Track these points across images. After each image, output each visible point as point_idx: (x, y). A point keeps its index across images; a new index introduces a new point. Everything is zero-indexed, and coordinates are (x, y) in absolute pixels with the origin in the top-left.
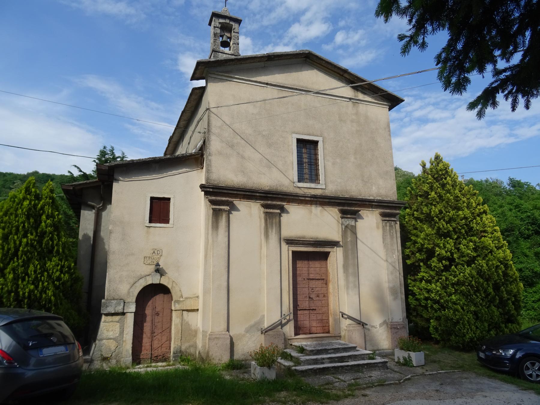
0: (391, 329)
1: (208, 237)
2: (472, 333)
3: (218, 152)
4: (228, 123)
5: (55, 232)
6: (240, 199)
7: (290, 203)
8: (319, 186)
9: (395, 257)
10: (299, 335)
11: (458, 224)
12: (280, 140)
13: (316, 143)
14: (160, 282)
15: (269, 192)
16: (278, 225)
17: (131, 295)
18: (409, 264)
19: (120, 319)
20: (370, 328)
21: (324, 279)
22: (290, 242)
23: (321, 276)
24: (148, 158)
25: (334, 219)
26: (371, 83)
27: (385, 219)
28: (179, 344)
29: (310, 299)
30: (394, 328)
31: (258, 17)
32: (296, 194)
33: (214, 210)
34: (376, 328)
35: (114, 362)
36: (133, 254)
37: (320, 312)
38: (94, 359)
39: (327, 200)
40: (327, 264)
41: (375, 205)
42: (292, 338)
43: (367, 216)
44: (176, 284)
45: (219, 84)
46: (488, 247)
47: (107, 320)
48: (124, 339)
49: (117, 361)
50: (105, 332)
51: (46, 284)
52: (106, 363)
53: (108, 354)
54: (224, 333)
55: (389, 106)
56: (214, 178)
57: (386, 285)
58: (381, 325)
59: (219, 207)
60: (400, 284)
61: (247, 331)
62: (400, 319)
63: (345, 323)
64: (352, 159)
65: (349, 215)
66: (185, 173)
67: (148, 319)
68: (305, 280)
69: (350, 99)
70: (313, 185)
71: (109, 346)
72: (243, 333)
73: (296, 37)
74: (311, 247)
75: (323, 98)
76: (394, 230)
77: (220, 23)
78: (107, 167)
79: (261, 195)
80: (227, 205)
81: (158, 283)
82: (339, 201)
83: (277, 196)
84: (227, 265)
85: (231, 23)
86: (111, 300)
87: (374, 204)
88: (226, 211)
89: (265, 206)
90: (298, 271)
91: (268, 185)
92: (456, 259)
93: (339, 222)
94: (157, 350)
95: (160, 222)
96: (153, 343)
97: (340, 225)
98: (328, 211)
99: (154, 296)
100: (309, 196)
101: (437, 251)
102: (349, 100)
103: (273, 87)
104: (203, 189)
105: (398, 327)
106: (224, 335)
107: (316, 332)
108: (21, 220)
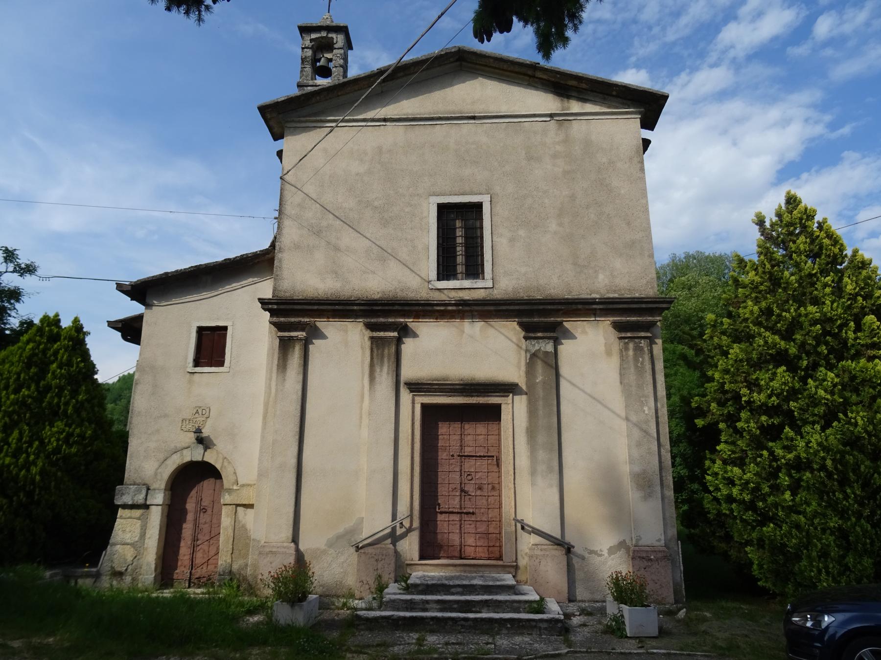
0: (633, 558)
1: (270, 385)
2: (830, 579)
3: (294, 244)
4: (314, 196)
5: (69, 386)
6: (328, 318)
7: (419, 318)
8: (479, 283)
9: (646, 412)
10: (439, 559)
11: (807, 334)
12: (406, 210)
13: (477, 207)
14: (203, 458)
15: (375, 302)
16: (393, 359)
17: (159, 477)
18: (701, 426)
19: (142, 515)
20: (587, 555)
21: (493, 456)
22: (416, 387)
23: (488, 450)
24: (189, 268)
25: (509, 342)
26: (399, 65)
27: (623, 335)
28: (229, 561)
29: (463, 494)
30: (639, 557)
31: (656, 30)
32: (426, 302)
33: (281, 339)
34: (601, 555)
35: (128, 579)
36: (166, 416)
37: (484, 519)
38: (102, 572)
39: (492, 308)
40: (499, 429)
41: (600, 309)
42: (412, 562)
43: (584, 332)
44: (229, 463)
45: (301, 135)
46: (874, 380)
47: (124, 515)
48: (146, 546)
49: (134, 579)
50: (120, 532)
51: (32, 457)
52: (117, 580)
53: (121, 567)
54: (285, 544)
55: (640, 113)
56: (285, 287)
57: (626, 469)
58: (611, 551)
59: (289, 333)
60: (661, 469)
61: (331, 544)
62: (659, 540)
63: (528, 541)
64: (553, 226)
65: (539, 332)
66: (252, 284)
67: (190, 517)
68: (455, 457)
69: (551, 116)
70: (467, 283)
71: (124, 555)
72: (323, 547)
73: (732, 47)
74: (459, 396)
75: (494, 125)
76: (647, 357)
77: (311, 40)
78: (130, 287)
79: (362, 308)
80: (303, 330)
81: (200, 460)
82: (517, 307)
83: (391, 308)
84: (298, 430)
85: (330, 35)
86: (131, 485)
87: (595, 306)
88: (301, 340)
89: (370, 327)
90: (440, 441)
91: (379, 290)
92: (794, 411)
93: (521, 348)
94: (201, 567)
95: (211, 365)
96: (194, 556)
97: (523, 353)
98: (496, 327)
99: (201, 482)
100: (453, 302)
101: (745, 396)
102: (548, 119)
103: (397, 124)
104: (266, 307)
105: (652, 557)
106: (284, 547)
107: (472, 555)
108: (14, 369)
